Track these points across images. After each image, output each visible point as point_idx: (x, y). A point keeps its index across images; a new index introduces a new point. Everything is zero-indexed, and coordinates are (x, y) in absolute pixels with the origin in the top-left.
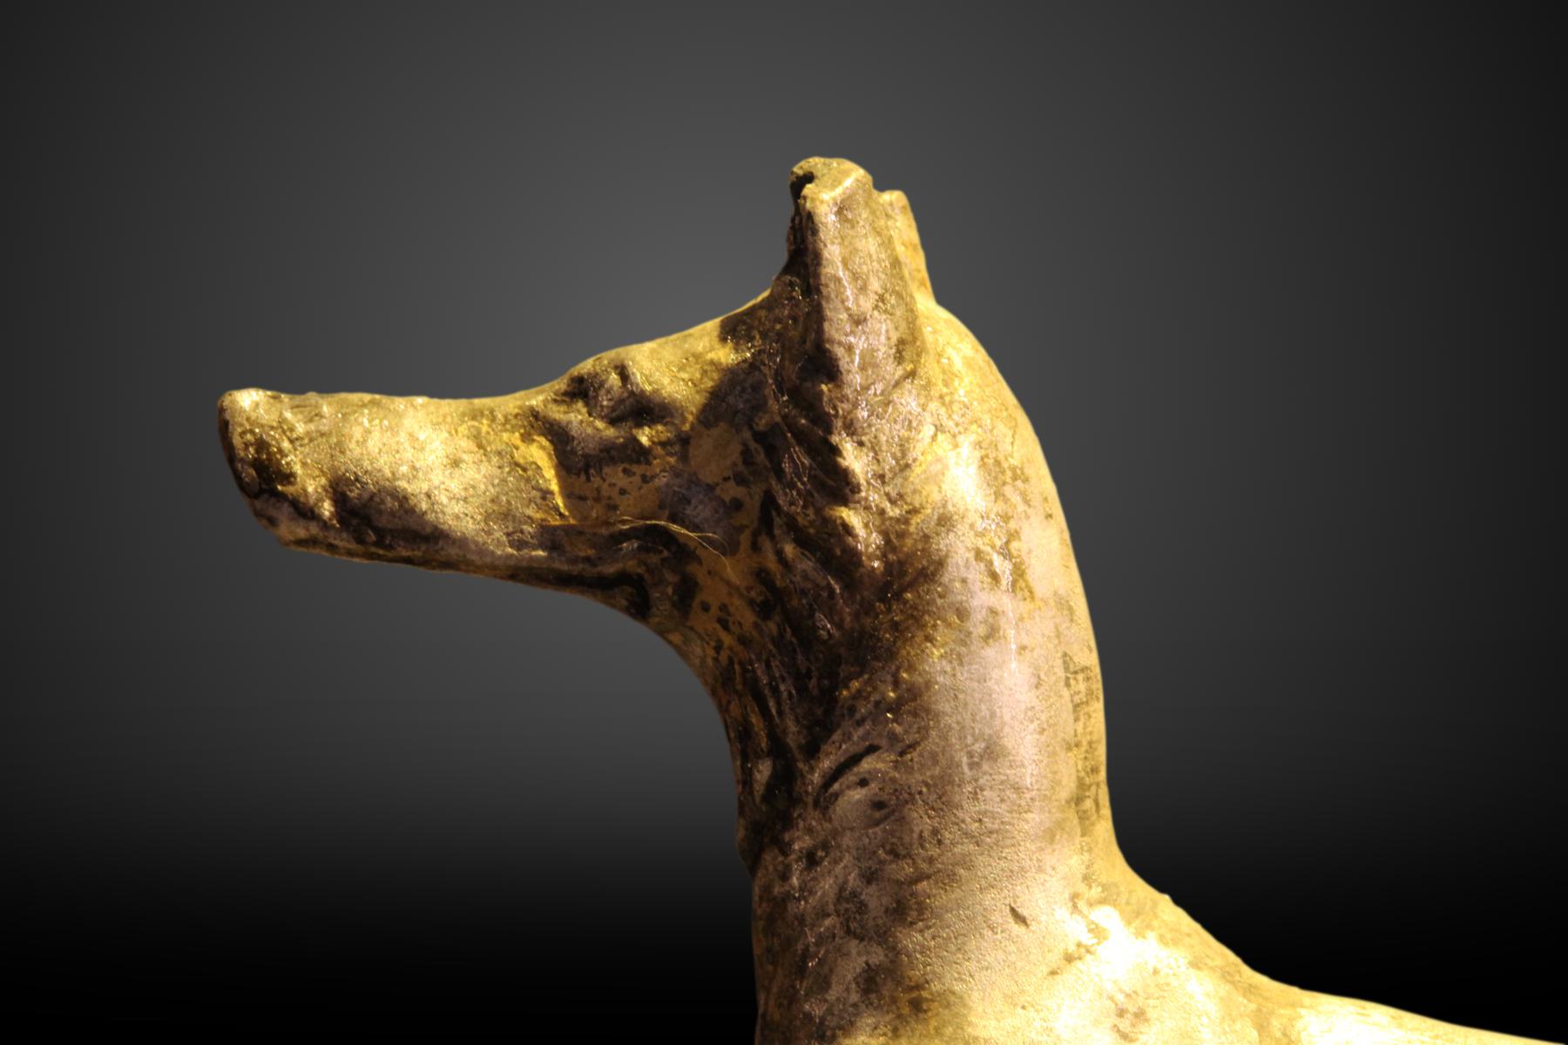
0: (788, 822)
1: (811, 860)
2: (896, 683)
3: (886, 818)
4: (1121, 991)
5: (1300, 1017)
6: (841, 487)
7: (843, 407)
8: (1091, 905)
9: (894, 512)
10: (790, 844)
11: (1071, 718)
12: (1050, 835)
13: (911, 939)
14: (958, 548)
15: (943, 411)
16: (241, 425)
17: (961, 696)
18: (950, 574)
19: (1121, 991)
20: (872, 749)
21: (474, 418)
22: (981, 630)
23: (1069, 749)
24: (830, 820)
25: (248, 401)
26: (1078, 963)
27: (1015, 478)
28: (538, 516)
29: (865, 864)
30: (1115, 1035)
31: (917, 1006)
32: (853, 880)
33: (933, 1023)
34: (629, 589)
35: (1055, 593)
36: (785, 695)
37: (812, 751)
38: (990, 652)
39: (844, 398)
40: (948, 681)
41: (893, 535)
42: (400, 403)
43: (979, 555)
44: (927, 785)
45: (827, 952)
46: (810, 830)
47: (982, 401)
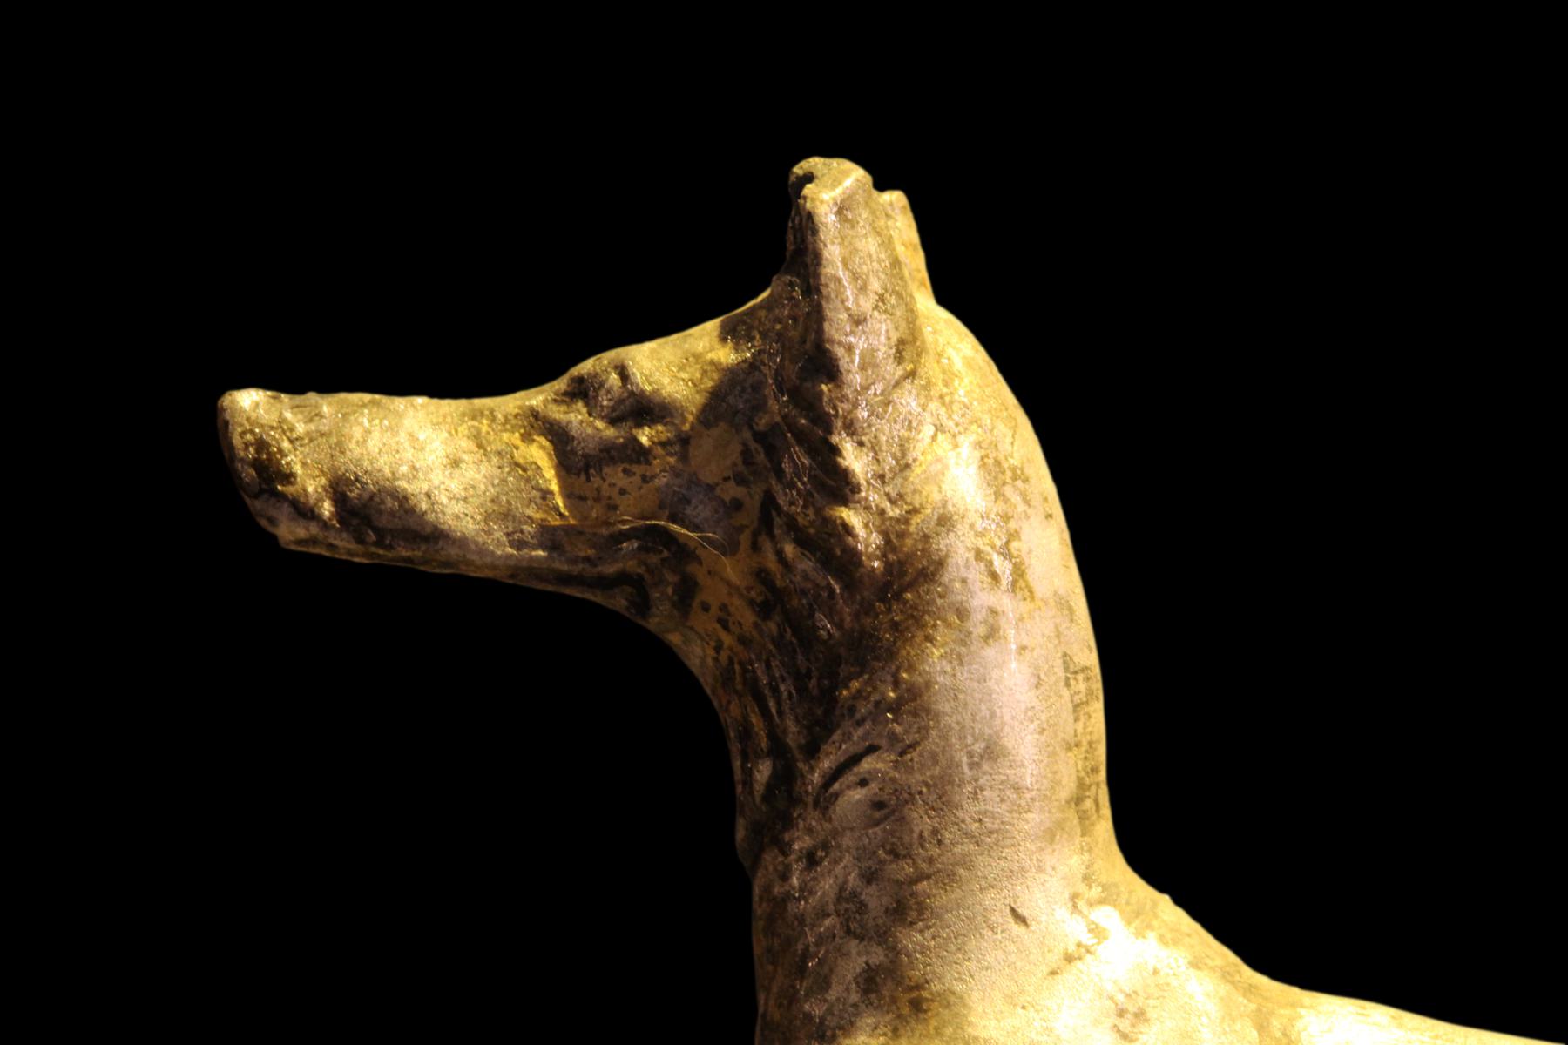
0: (788, 822)
1: (811, 860)
2: (896, 683)
3: (886, 818)
4: (1121, 991)
5: (1300, 1017)
6: (841, 487)
7: (843, 407)
8: (1091, 905)
9: (894, 512)
10: (790, 844)
11: (1071, 718)
12: (1050, 835)
13: (911, 939)
14: (958, 548)
15: (943, 411)
16: (241, 425)
17: (961, 696)
18: (950, 574)
19: (1121, 991)
20: (872, 749)
21: (474, 418)
22: (981, 630)
23: (1069, 749)
24: (830, 820)
25: (248, 402)
26: (1078, 963)
27: (1015, 478)
28: (538, 516)
29: (865, 864)
30: (1115, 1035)
31: (917, 1006)
32: (853, 880)
33: (933, 1023)
34: (629, 589)
35: (1055, 593)
36: (785, 695)
37: (812, 751)
38: (990, 652)
39: (844, 398)
40: (948, 681)
41: (893, 535)
42: (400, 403)
43: (979, 555)
44: (927, 785)
45: (827, 952)
46: (810, 830)
47: (982, 401)
